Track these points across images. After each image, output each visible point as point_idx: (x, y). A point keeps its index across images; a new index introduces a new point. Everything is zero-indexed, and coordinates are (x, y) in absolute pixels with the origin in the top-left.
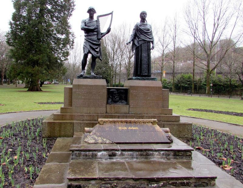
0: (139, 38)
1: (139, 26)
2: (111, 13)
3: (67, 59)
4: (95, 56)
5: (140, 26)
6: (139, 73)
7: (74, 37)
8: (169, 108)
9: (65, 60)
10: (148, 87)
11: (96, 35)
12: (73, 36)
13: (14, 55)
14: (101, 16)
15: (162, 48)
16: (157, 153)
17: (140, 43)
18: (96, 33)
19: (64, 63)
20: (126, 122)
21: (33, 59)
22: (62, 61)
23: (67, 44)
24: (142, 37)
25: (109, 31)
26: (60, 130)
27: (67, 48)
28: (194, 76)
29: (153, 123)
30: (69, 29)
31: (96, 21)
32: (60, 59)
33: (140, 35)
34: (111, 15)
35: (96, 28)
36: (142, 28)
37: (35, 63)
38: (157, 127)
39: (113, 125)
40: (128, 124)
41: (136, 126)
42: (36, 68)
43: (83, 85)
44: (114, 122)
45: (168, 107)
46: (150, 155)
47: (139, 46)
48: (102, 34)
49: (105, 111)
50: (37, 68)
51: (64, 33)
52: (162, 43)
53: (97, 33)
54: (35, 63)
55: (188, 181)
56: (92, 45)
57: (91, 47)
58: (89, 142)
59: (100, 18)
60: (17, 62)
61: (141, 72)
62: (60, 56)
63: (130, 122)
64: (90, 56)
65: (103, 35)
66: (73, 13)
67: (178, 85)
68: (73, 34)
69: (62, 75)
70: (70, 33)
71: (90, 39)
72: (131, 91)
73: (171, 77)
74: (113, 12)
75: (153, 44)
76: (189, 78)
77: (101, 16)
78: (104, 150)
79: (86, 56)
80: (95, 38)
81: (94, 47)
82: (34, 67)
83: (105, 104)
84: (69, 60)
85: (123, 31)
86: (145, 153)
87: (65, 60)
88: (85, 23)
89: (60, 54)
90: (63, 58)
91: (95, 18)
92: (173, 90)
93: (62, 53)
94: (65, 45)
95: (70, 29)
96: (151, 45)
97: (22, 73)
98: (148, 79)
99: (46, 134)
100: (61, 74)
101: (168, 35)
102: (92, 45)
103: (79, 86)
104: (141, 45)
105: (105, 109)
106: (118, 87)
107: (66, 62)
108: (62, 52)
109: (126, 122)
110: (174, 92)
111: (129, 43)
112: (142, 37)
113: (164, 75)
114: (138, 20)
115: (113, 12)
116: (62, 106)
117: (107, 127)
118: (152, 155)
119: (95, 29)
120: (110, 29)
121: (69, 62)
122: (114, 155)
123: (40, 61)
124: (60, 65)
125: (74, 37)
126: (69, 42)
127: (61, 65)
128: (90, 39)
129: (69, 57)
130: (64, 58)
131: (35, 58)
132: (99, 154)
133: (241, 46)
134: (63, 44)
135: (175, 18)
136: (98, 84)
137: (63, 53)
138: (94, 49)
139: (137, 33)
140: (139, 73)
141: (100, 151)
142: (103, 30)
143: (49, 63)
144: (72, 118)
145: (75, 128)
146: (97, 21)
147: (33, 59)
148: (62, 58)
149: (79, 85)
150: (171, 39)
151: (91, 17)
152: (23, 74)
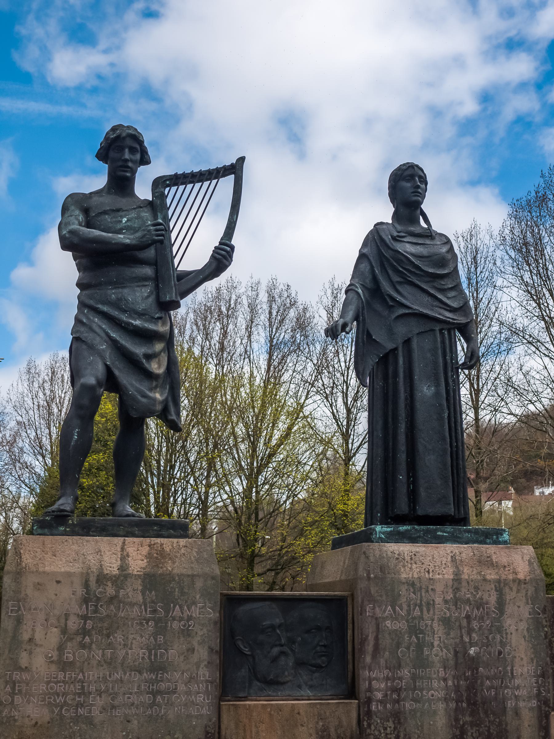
1: (387, 238)
2: (236, 169)
4: (144, 400)
5: (394, 239)
11: (146, 279)
13: (83, 273)
18: (148, 271)
25: (222, 258)
31: (150, 204)
33: (399, 287)
34: (228, 182)
35: (154, 242)
36: (407, 248)
53: (157, 272)
57: (115, 344)
59: (171, 192)
64: (108, 406)
66: (180, 172)
71: (116, 305)
74: (242, 160)
75: (468, 340)
80: (140, 296)
81: (139, 350)
91: (143, 191)
96: (461, 348)
98: (455, 539)
104: (407, 342)
106: (254, 704)
111: (344, 326)
115: (242, 160)
119: (142, 246)
120: (232, 248)
128: (116, 305)
139: (380, 278)
142: (192, 255)
146: (157, 206)
151: (121, 183)
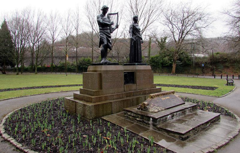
2: (117, 13)
6: (137, 60)
8: (154, 83)
10: (145, 70)
11: (109, 29)
16: (187, 110)
17: (136, 38)
18: (109, 28)
26: (103, 110)
28: (92, 59)
40: (164, 96)
41: (168, 96)
43: (110, 71)
45: (153, 83)
47: (136, 41)
48: (113, 29)
49: (123, 91)
55: (99, 146)
58: (155, 111)
67: (80, 67)
73: (75, 60)
76: (89, 61)
78: (170, 114)
83: (123, 85)
85: (26, 16)
92: (77, 70)
99: (93, 116)
101: (71, 25)
105: (123, 88)
110: (77, 72)
113: (67, 59)
114: (132, 22)
116: (82, 87)
118: (186, 111)
132: (168, 117)
135: (77, 12)
136: (108, 69)
140: (137, 60)
141: (168, 115)
144: (106, 98)
145: (113, 106)
149: (107, 71)
150: (73, 28)
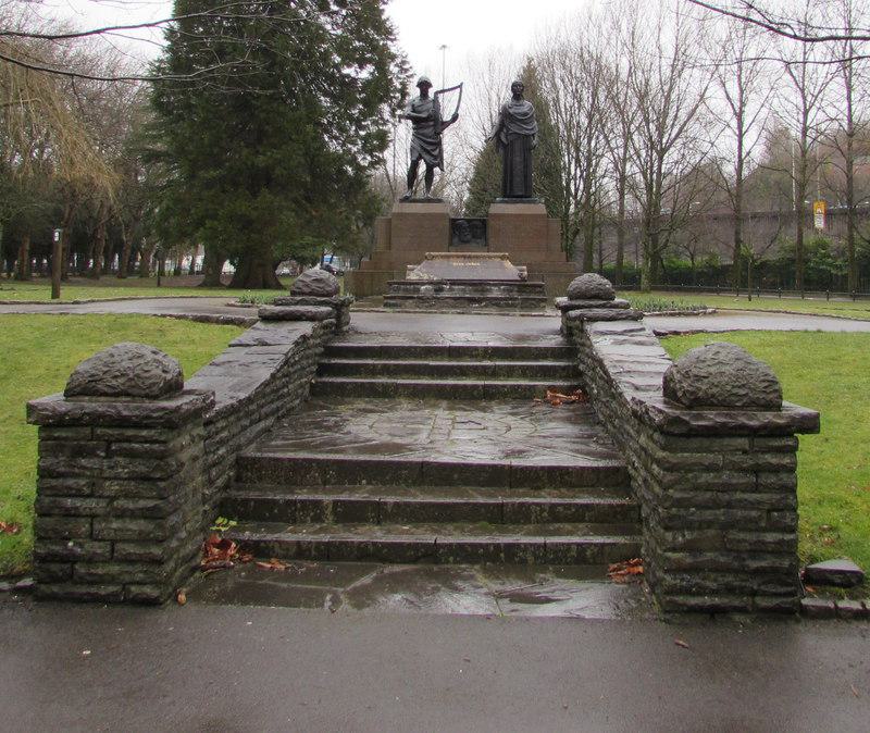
0: (508, 130)
2: (460, 86)
3: (382, 161)
7: (409, 73)
9: (372, 165)
12: (403, 70)
14: (443, 91)
15: (799, 101)
18: (432, 123)
19: (368, 176)
20: (465, 257)
21: (253, 165)
22: (359, 168)
23: (381, 100)
24: (514, 128)
25: (455, 118)
27: (382, 118)
29: (503, 258)
30: (389, 43)
32: (353, 162)
37: (261, 180)
38: (508, 264)
39: (445, 261)
42: (266, 196)
44: (448, 257)
46: (487, 290)
50: (269, 197)
51: (370, 61)
52: (799, 79)
54: (261, 180)
56: (425, 146)
59: (440, 96)
60: (192, 176)
61: (511, 190)
62: (355, 149)
63: (470, 257)
65: (445, 125)
68: (404, 62)
69: (361, 225)
70: (393, 57)
72: (491, 223)
77: (443, 91)
79: (415, 165)
80: (429, 131)
82: (255, 195)
84: (389, 165)
86: (480, 288)
87: (372, 165)
88: (413, 106)
89: (355, 144)
90: (364, 158)
93: (362, 138)
94: (371, 107)
95: (392, 40)
97: (214, 217)
100: (358, 218)
102: (425, 146)
103: (401, 216)
107: (378, 172)
108: (362, 133)
109: (465, 257)
112: (514, 128)
117: (437, 262)
121: (391, 173)
122: (441, 290)
123: (278, 171)
124: (351, 184)
125: (409, 73)
126: (388, 91)
127: (359, 182)
129: (387, 154)
130: (369, 158)
131: (261, 161)
133: (865, 118)
134: (366, 103)
137: (366, 139)
138: (428, 152)
141: (424, 284)
143: (308, 179)
146: (435, 100)
147: (253, 165)
148: (360, 158)
152: (216, 223)
